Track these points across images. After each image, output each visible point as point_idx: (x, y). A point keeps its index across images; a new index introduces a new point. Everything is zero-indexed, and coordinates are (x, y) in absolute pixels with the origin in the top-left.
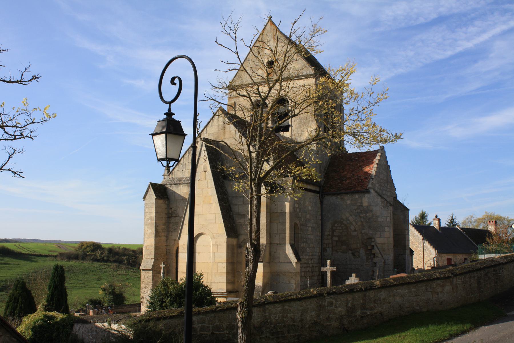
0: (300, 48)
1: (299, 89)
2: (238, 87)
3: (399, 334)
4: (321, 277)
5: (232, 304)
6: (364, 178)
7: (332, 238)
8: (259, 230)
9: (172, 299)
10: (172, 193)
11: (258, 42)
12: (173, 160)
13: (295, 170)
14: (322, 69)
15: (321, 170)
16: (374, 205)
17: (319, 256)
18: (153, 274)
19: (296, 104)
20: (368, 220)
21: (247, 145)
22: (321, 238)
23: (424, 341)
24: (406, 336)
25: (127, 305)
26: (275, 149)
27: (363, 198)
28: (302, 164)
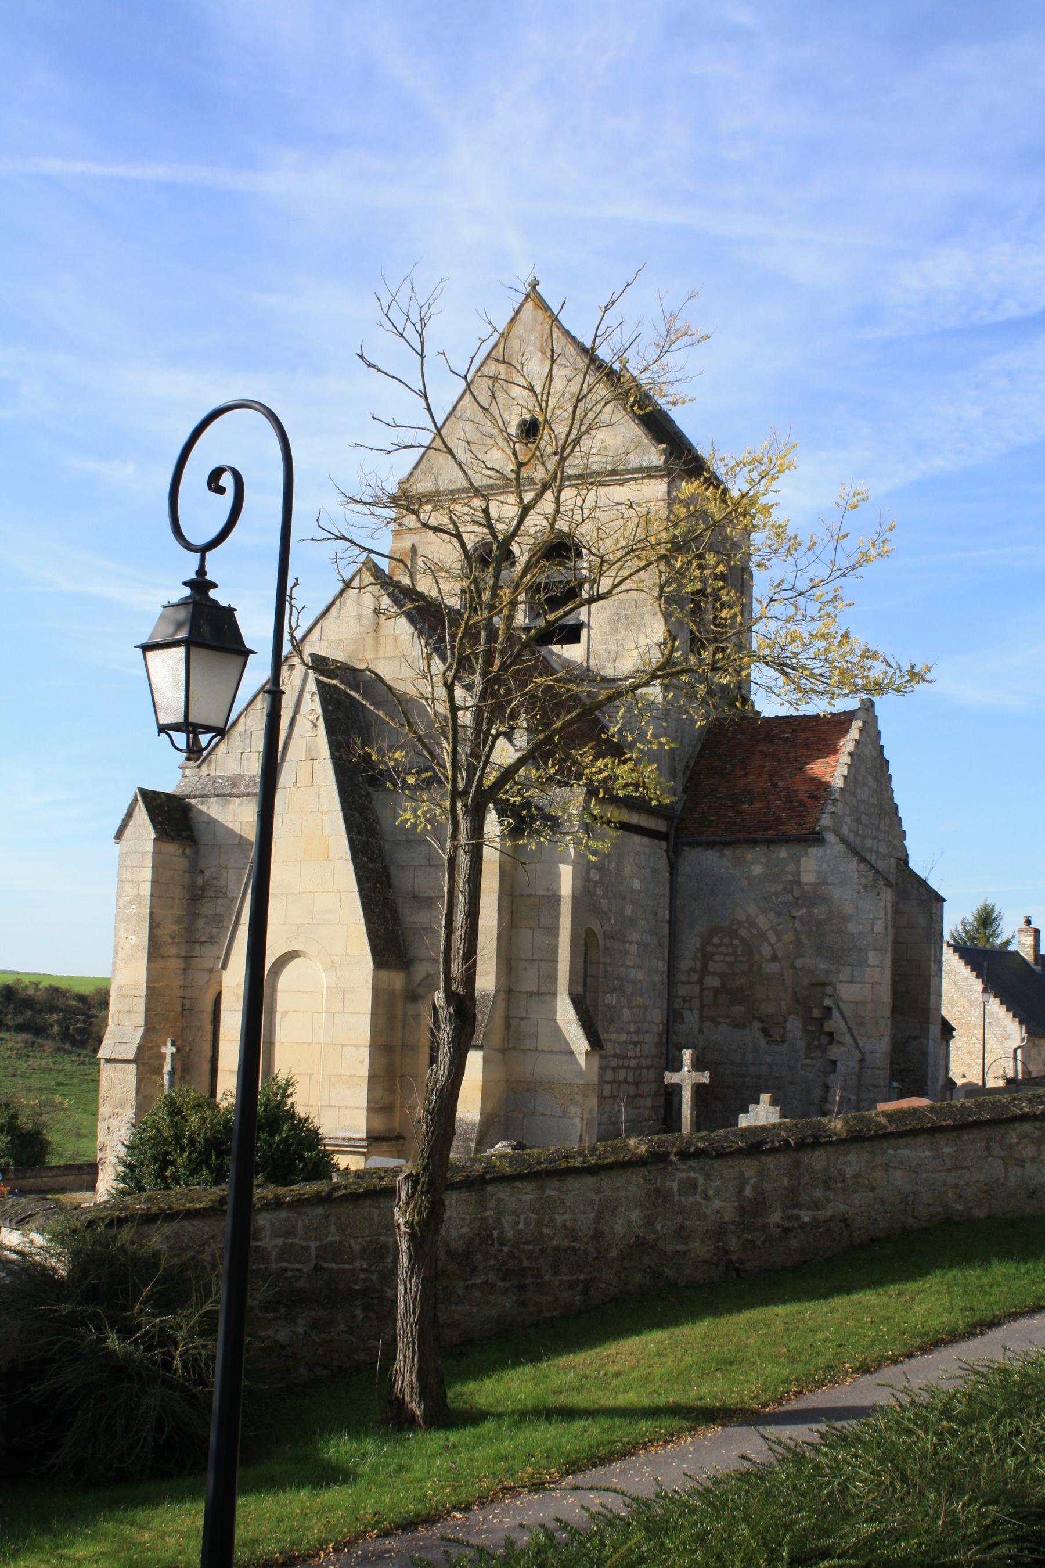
0: (621, 387)
1: (613, 514)
2: (423, 499)
3: (897, 1287)
4: (662, 1099)
5: (381, 1178)
6: (809, 797)
7: (700, 981)
8: (475, 953)
9: (194, 1156)
10: (209, 823)
11: (490, 361)
12: (208, 729)
13: (593, 766)
14: (690, 451)
15: (675, 769)
16: (836, 881)
17: (660, 1035)
18: (137, 1074)
19: (602, 562)
20: (814, 929)
21: (445, 684)
22: (668, 977)
23: (974, 1311)
24: (919, 1293)
25: (54, 1167)
26: (532, 700)
27: (803, 859)
28: (616, 750)
